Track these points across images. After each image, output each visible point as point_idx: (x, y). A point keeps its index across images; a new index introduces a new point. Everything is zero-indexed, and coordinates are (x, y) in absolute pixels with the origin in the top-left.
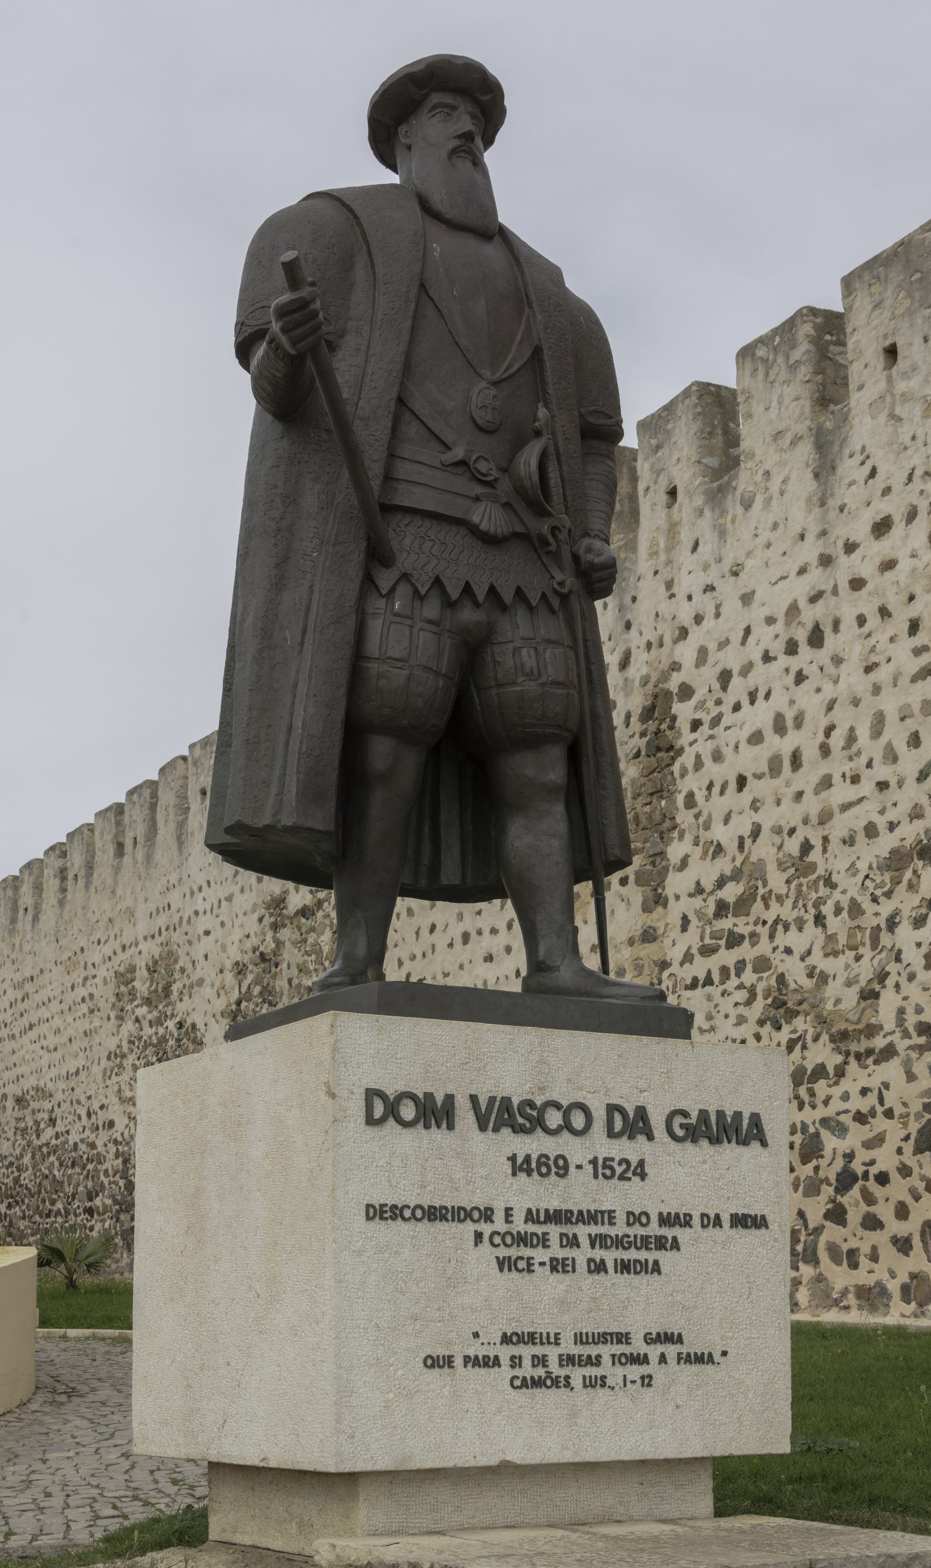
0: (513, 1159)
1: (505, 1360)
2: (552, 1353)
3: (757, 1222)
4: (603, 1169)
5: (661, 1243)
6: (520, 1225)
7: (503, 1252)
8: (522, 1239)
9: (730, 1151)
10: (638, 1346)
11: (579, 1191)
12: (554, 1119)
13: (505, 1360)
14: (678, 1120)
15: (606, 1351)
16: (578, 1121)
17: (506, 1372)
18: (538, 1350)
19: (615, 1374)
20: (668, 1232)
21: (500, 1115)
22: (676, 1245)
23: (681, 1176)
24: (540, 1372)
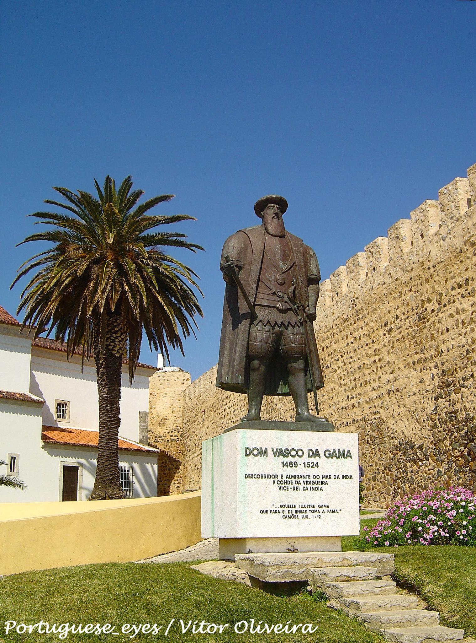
0: (283, 463)
1: (281, 512)
2: (294, 510)
3: (350, 477)
4: (307, 465)
5: (323, 483)
6: (284, 479)
7: (280, 485)
8: (285, 482)
9: (342, 460)
10: (317, 508)
11: (301, 470)
12: (293, 453)
13: (281, 512)
14: (327, 453)
15: (308, 509)
16: (300, 453)
17: (281, 514)
18: (290, 509)
19: (310, 515)
20: (325, 480)
21: (280, 453)
22: (327, 483)
23: (327, 466)
24: (291, 514)
